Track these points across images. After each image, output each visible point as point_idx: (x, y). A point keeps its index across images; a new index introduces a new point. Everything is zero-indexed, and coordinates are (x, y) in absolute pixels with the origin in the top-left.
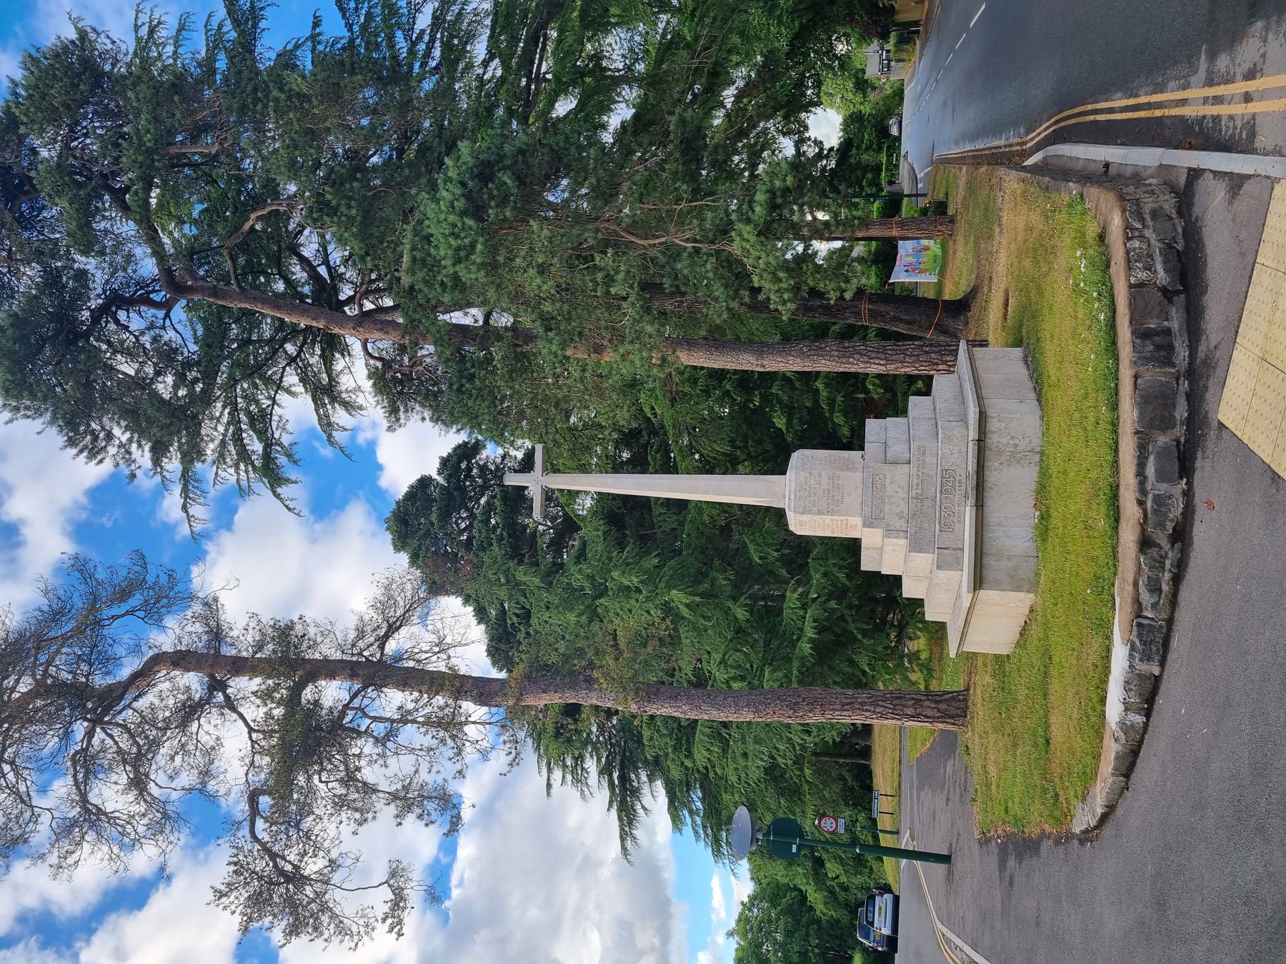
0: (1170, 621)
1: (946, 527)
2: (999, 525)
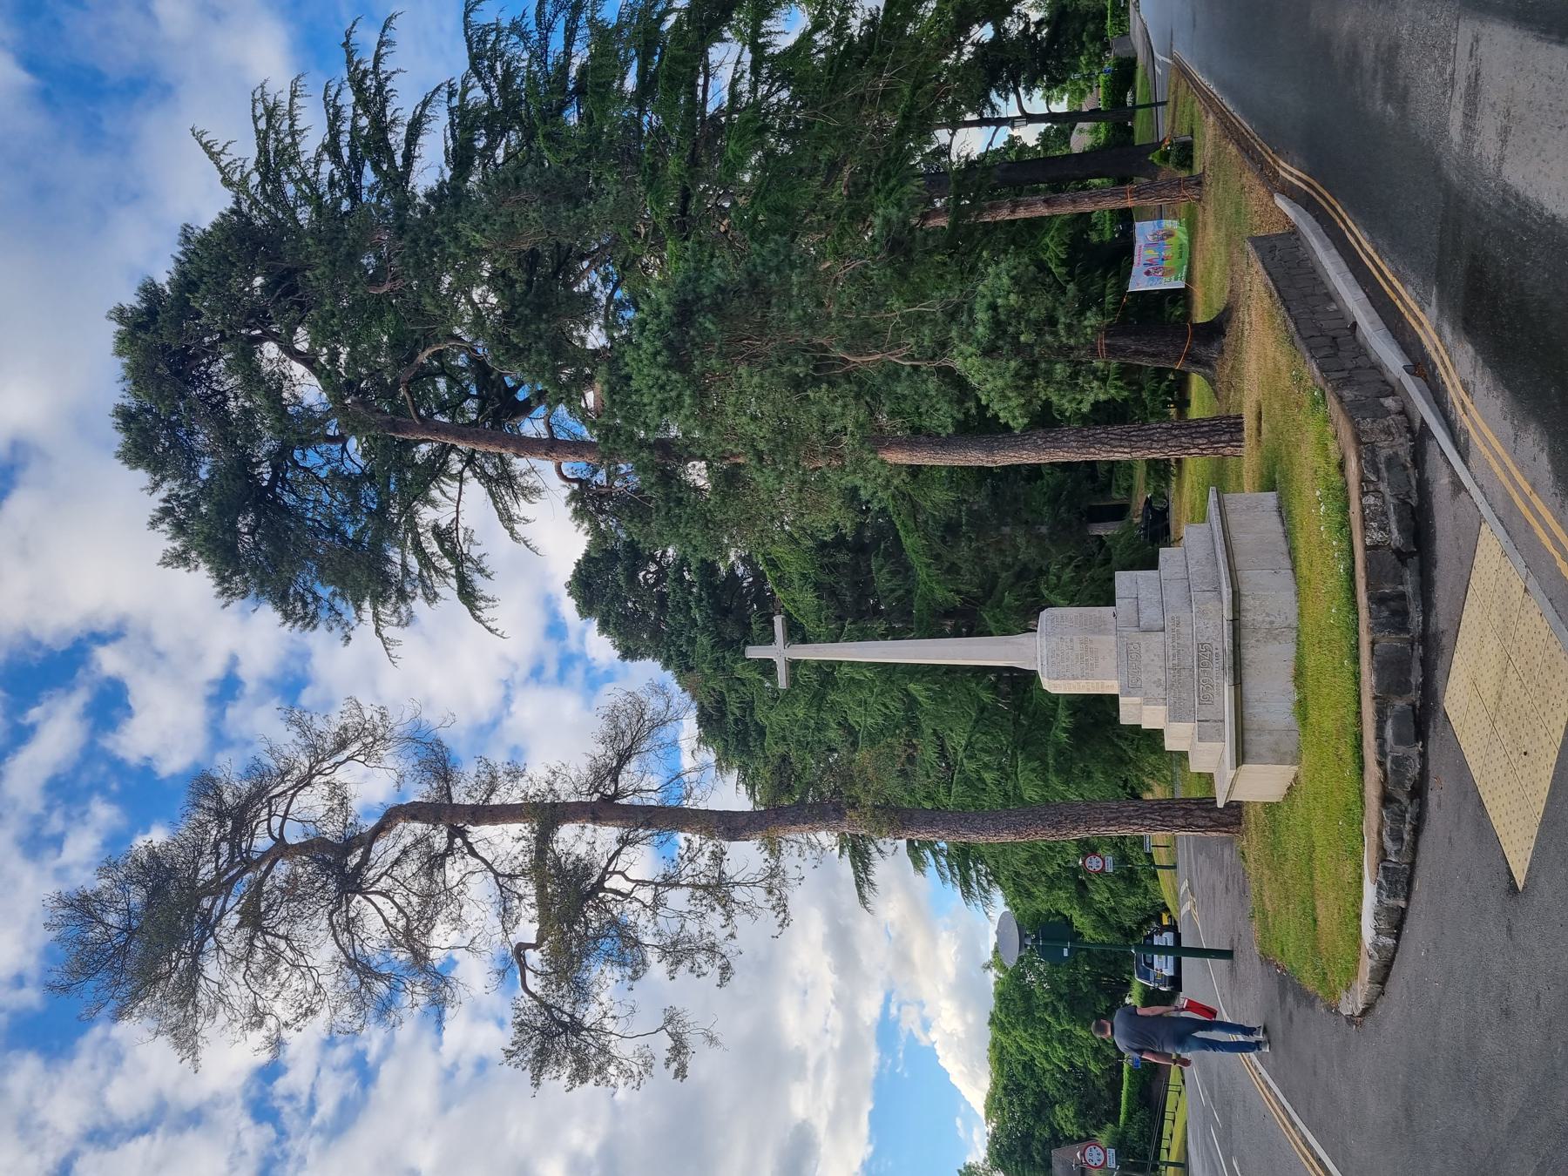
0: (1413, 865)
1: (1205, 700)
2: (1259, 701)
